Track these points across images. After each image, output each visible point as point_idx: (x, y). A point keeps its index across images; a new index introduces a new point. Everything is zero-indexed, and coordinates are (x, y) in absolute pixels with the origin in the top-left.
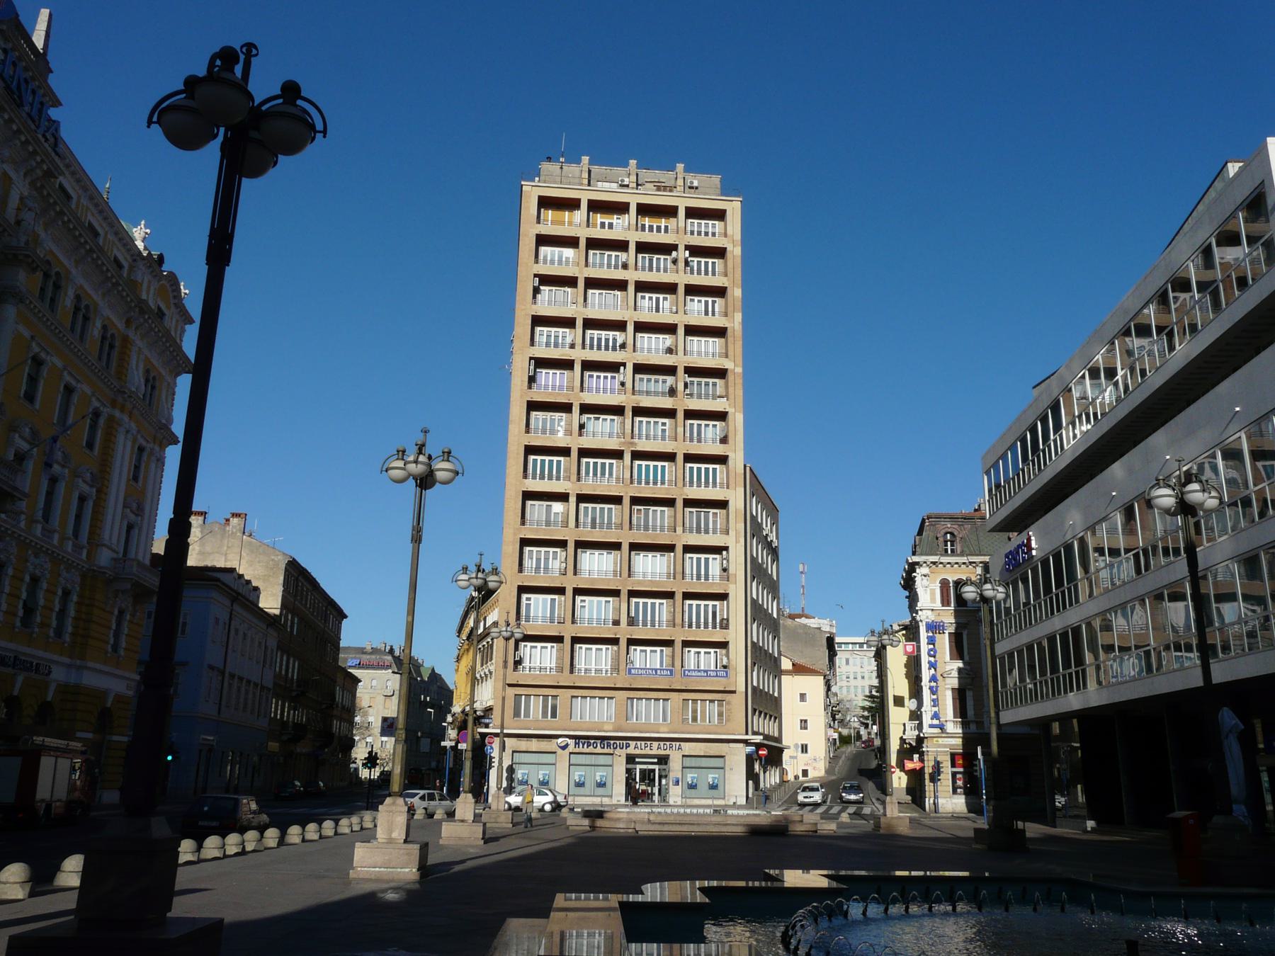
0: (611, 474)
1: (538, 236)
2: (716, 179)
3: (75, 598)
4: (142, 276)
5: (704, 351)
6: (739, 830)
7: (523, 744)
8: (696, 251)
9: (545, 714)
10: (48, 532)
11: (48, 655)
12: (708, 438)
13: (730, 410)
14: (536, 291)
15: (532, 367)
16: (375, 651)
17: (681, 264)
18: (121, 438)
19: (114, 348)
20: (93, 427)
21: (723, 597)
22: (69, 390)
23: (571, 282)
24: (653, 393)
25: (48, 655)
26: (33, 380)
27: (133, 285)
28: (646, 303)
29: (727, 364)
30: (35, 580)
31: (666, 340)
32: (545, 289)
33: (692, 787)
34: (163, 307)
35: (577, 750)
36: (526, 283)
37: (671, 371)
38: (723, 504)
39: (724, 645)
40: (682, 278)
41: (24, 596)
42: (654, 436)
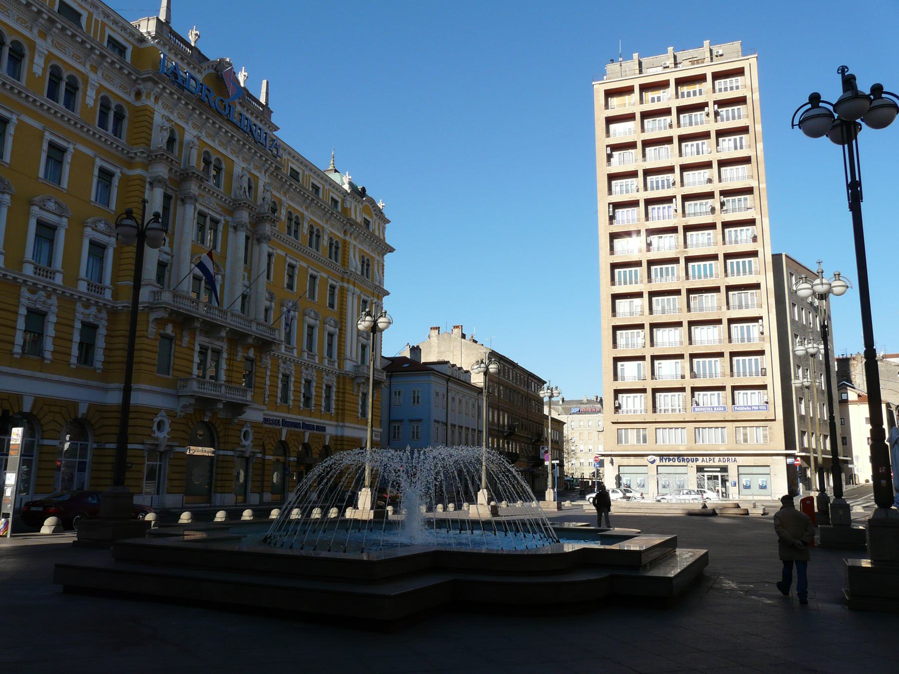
0: (673, 274)
1: (606, 118)
2: (737, 45)
3: (334, 389)
4: (350, 203)
5: (735, 177)
6: (678, 512)
7: (625, 461)
8: (722, 103)
9: (638, 440)
10: (312, 357)
11: (322, 421)
12: (741, 239)
13: (758, 217)
14: (609, 157)
15: (611, 209)
16: (589, 402)
17: (712, 115)
18: (350, 298)
19: (336, 249)
20: (332, 295)
21: (761, 353)
22: (313, 278)
23: (632, 145)
24: (698, 212)
25: (322, 421)
26: (291, 277)
27: (345, 210)
28: (688, 149)
29: (753, 183)
30: (308, 382)
31: (705, 173)
32: (616, 154)
33: (747, 487)
34: (367, 218)
35: (661, 464)
36: (601, 152)
37: (710, 195)
38: (757, 286)
39: (764, 387)
40: (712, 126)
41: (303, 391)
42: (700, 243)
